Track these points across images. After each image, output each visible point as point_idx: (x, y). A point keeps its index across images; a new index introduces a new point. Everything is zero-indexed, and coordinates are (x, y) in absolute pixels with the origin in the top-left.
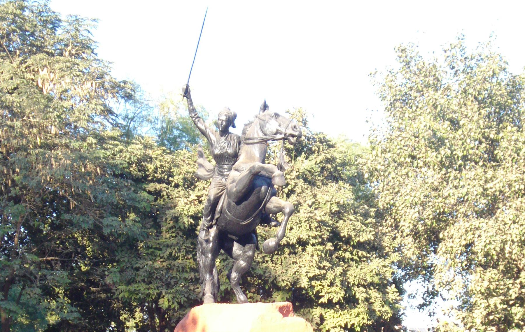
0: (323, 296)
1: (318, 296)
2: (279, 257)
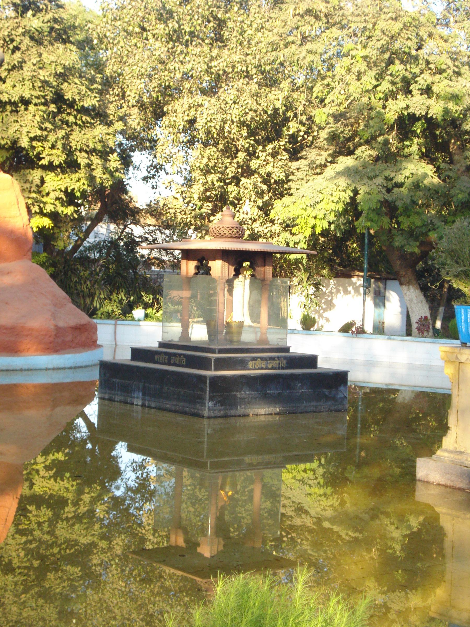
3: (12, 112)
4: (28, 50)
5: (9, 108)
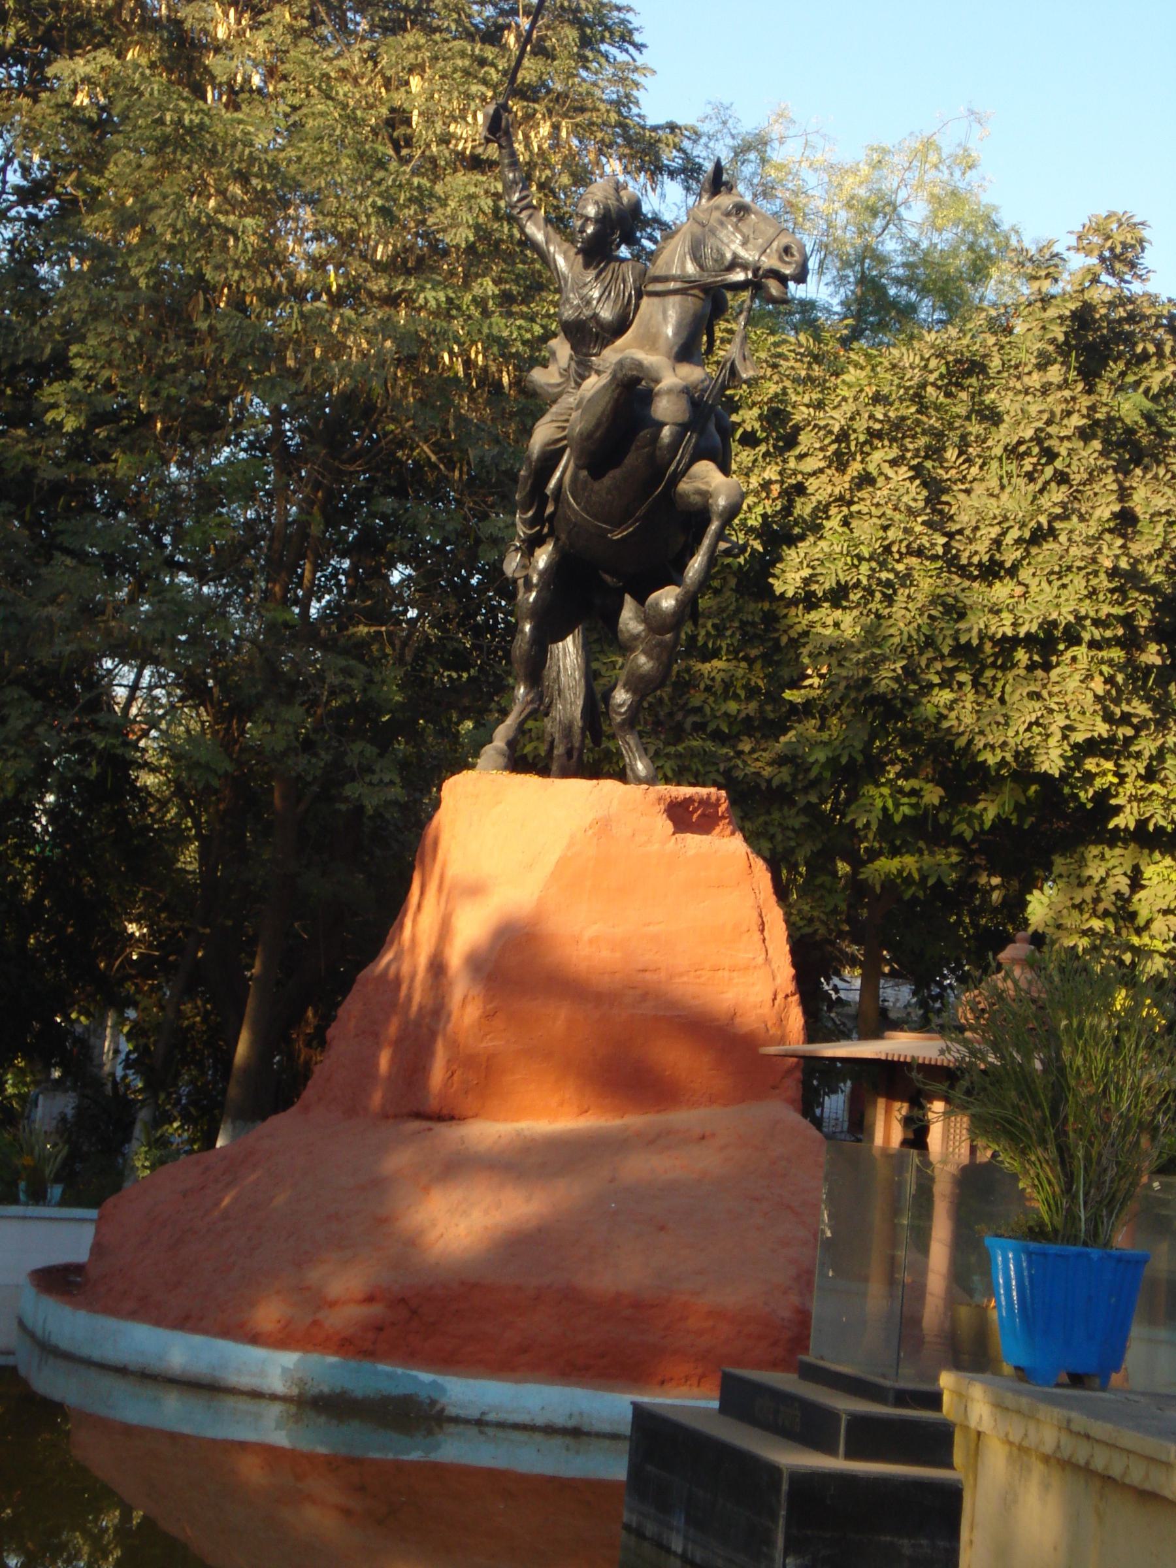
0: (1118, 809)
1: (1104, 806)
2: (1000, 675)
3: (1031, 668)
4: (1090, 480)
5: (1021, 655)
